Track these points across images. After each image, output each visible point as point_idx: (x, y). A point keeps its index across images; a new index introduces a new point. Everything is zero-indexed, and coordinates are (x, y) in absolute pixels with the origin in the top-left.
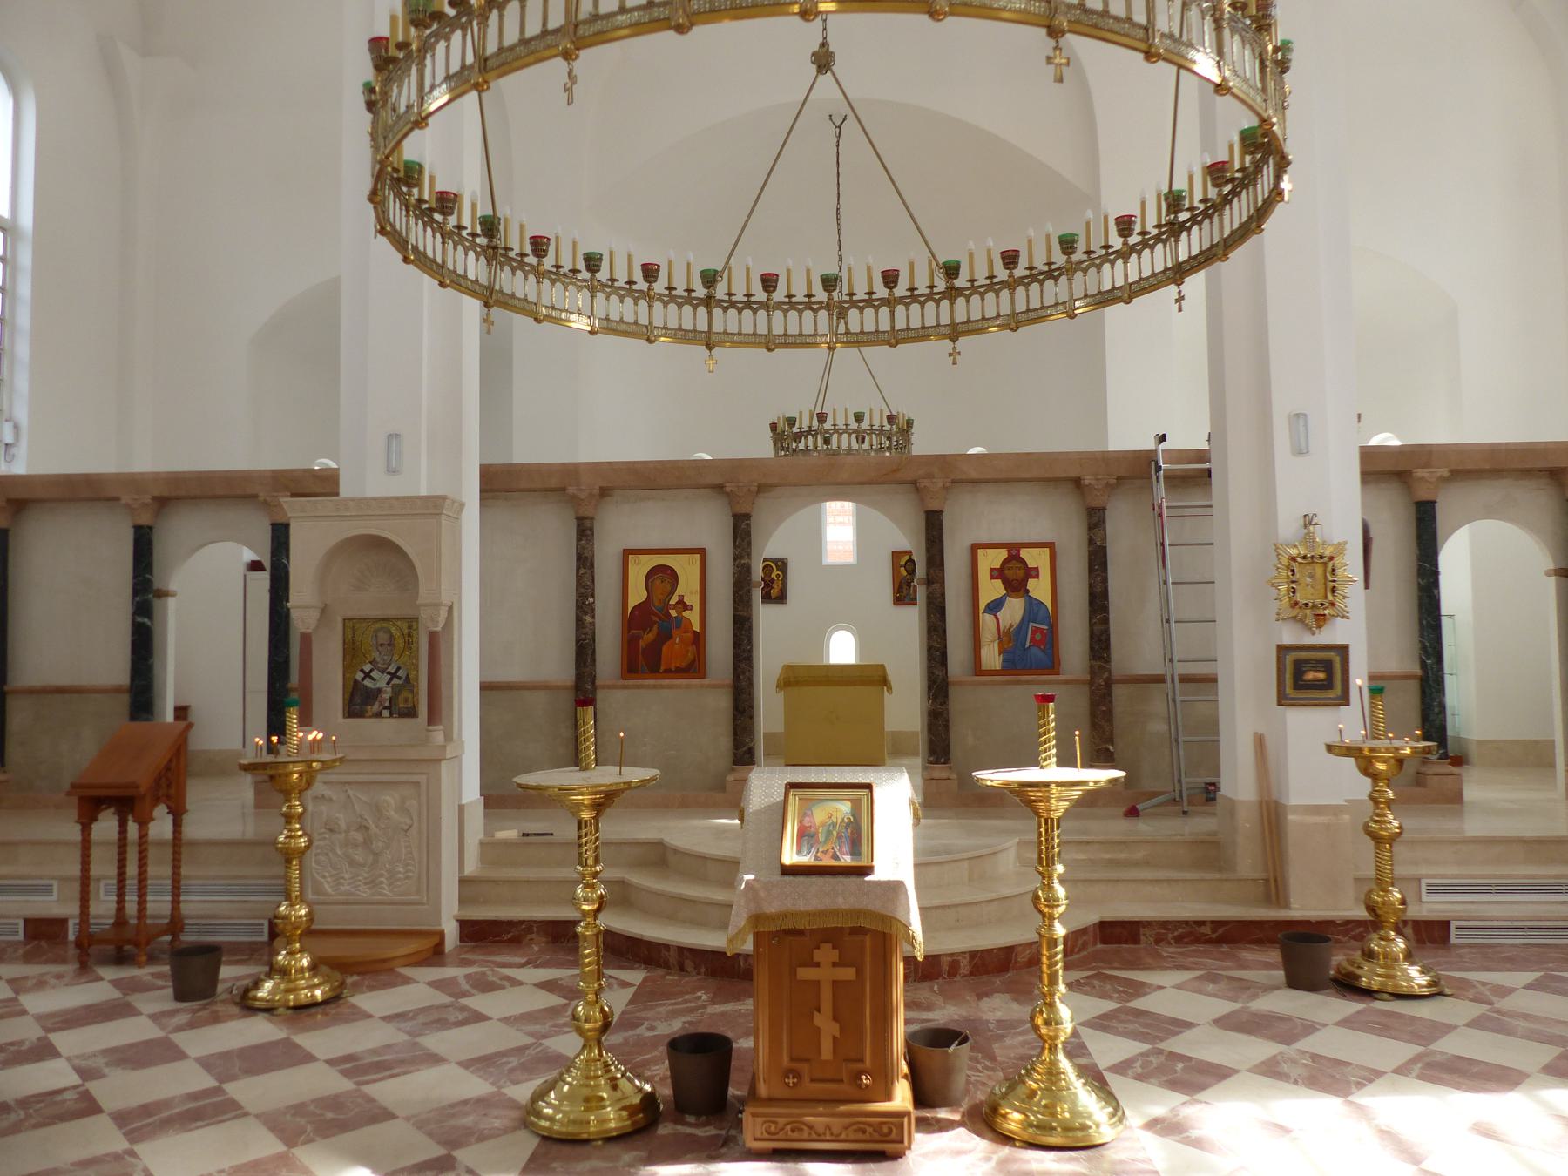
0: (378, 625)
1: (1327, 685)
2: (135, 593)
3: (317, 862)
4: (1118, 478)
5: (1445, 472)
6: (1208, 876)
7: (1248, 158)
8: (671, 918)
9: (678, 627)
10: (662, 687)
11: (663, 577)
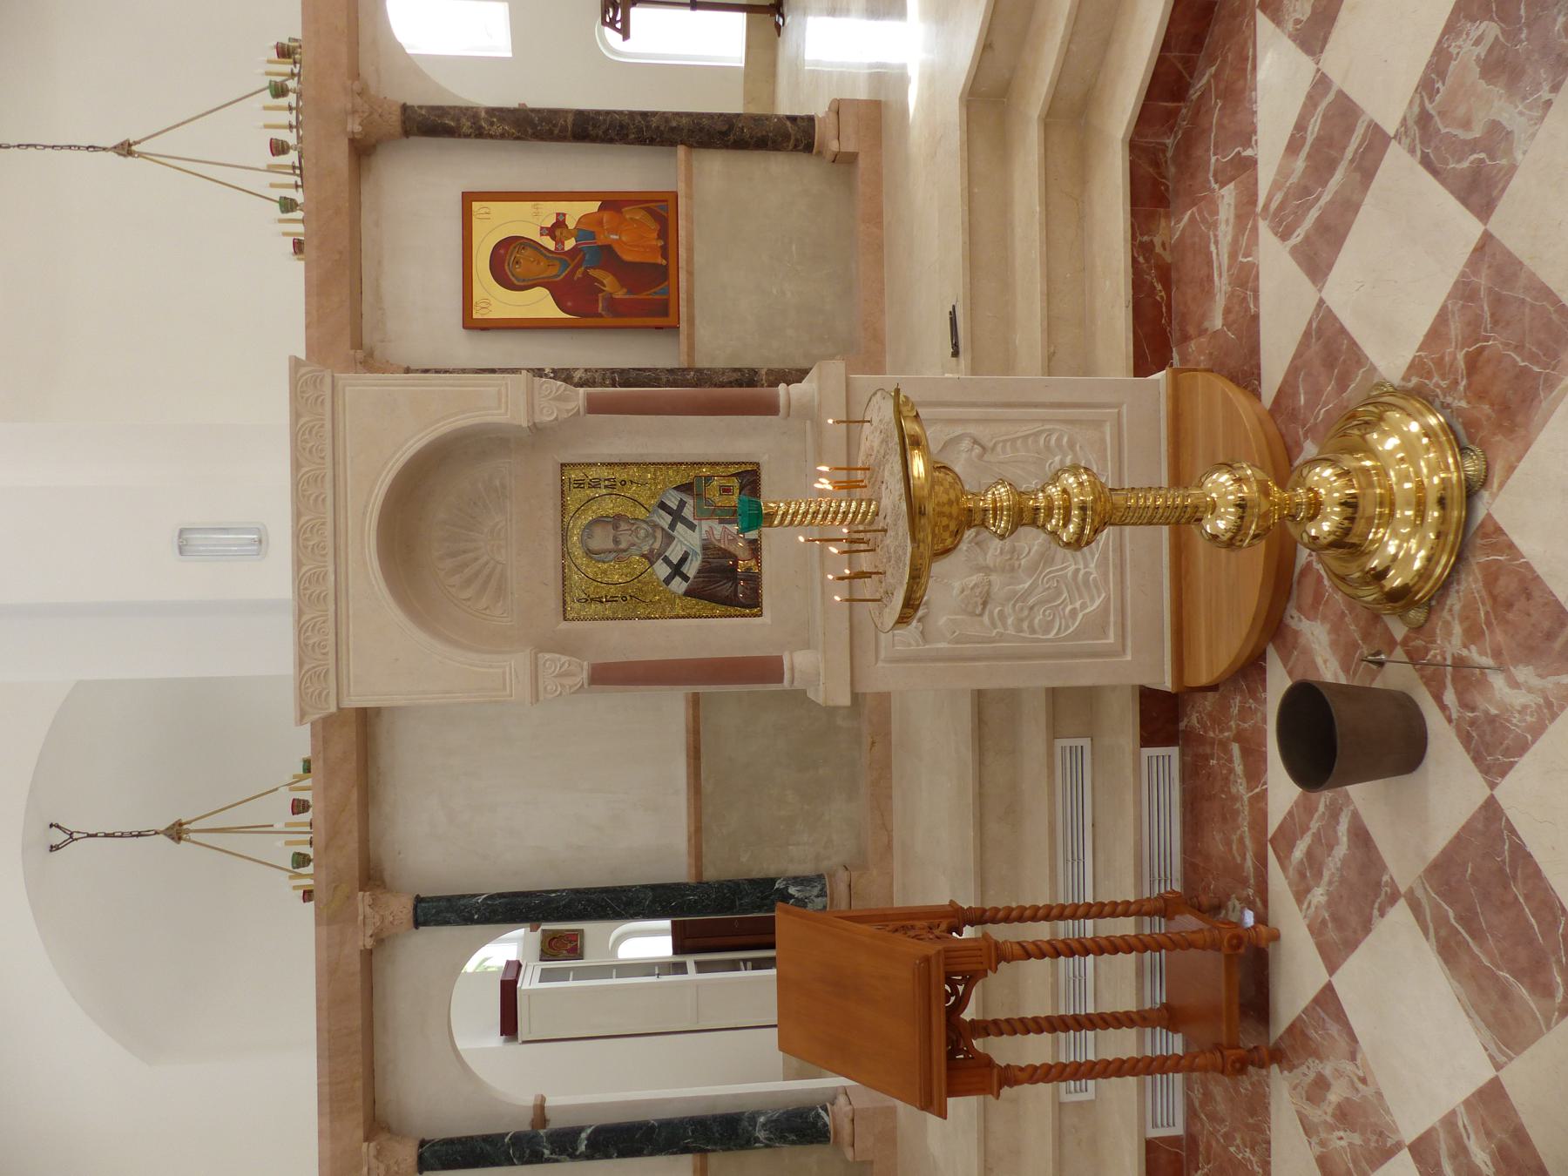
0: (578, 552)
2: (536, 1158)
3: (1047, 627)
9: (592, 235)
10: (690, 260)
11: (510, 263)
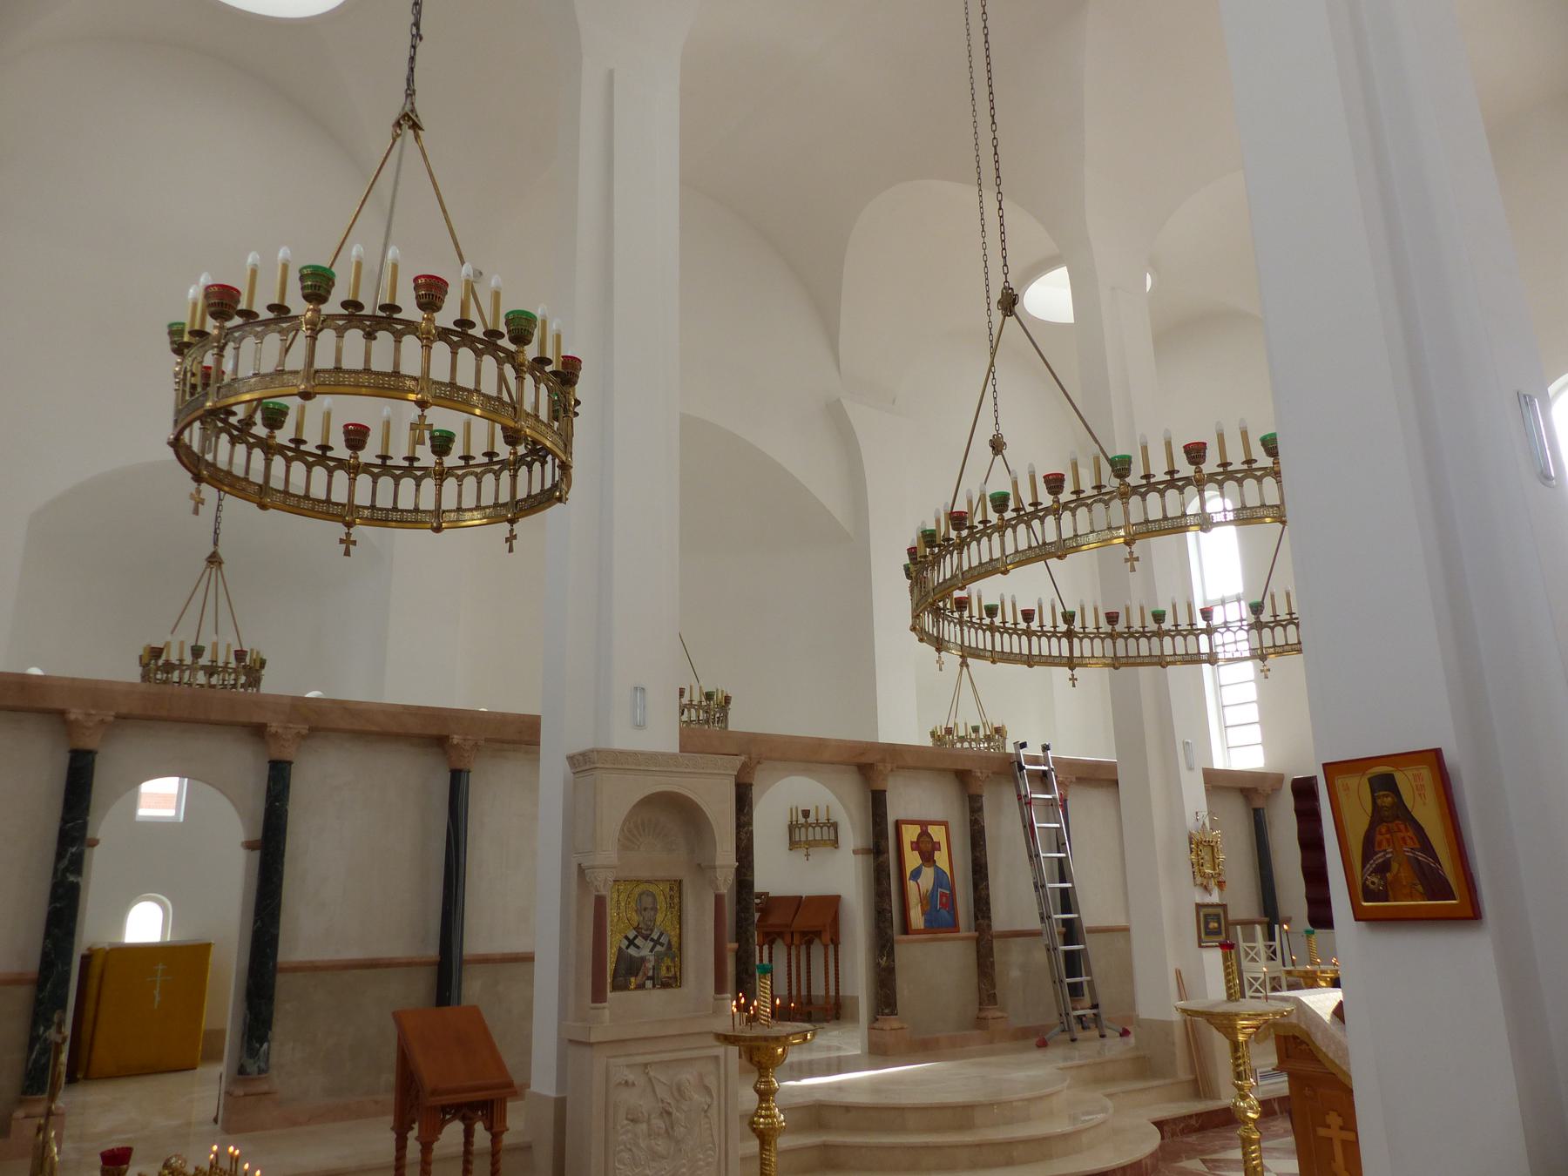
0: (643, 887)
4: (118, 717)
5: (303, 729)
6: (1155, 1083)
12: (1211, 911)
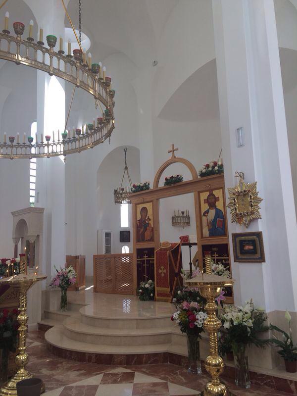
1: (254, 252)
7: (99, 125)
8: (119, 345)
12: (238, 251)
